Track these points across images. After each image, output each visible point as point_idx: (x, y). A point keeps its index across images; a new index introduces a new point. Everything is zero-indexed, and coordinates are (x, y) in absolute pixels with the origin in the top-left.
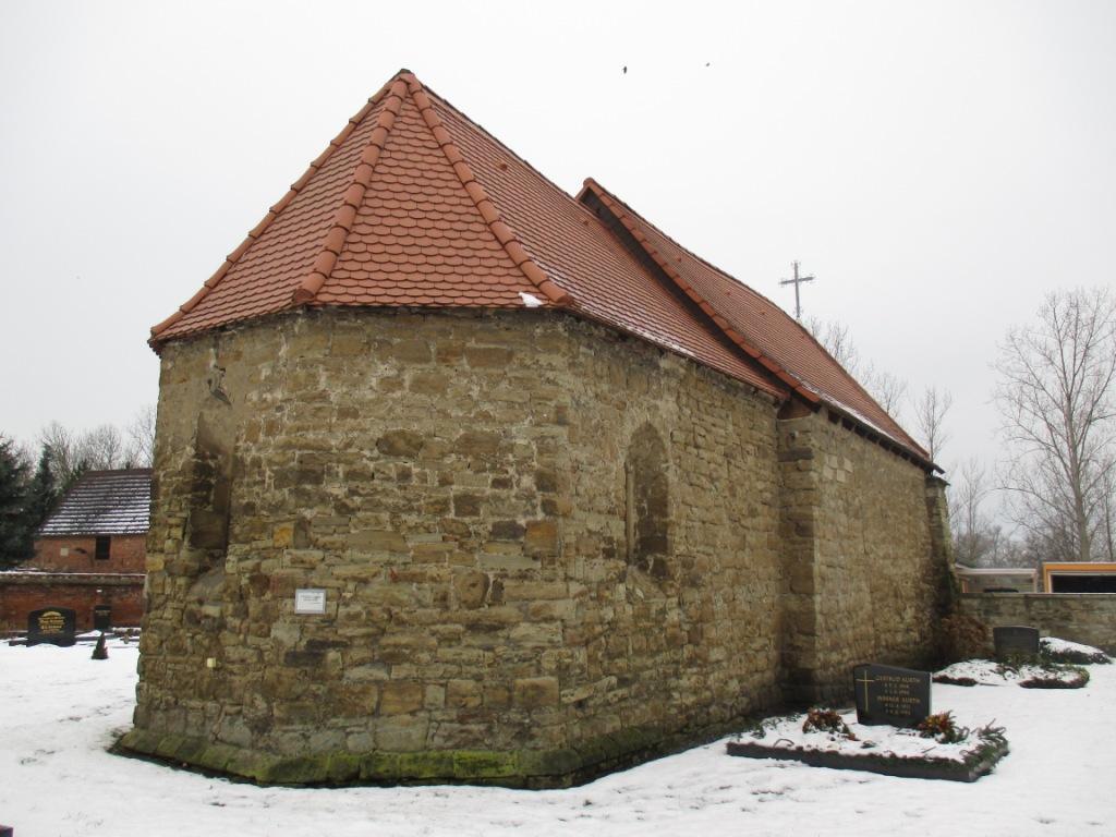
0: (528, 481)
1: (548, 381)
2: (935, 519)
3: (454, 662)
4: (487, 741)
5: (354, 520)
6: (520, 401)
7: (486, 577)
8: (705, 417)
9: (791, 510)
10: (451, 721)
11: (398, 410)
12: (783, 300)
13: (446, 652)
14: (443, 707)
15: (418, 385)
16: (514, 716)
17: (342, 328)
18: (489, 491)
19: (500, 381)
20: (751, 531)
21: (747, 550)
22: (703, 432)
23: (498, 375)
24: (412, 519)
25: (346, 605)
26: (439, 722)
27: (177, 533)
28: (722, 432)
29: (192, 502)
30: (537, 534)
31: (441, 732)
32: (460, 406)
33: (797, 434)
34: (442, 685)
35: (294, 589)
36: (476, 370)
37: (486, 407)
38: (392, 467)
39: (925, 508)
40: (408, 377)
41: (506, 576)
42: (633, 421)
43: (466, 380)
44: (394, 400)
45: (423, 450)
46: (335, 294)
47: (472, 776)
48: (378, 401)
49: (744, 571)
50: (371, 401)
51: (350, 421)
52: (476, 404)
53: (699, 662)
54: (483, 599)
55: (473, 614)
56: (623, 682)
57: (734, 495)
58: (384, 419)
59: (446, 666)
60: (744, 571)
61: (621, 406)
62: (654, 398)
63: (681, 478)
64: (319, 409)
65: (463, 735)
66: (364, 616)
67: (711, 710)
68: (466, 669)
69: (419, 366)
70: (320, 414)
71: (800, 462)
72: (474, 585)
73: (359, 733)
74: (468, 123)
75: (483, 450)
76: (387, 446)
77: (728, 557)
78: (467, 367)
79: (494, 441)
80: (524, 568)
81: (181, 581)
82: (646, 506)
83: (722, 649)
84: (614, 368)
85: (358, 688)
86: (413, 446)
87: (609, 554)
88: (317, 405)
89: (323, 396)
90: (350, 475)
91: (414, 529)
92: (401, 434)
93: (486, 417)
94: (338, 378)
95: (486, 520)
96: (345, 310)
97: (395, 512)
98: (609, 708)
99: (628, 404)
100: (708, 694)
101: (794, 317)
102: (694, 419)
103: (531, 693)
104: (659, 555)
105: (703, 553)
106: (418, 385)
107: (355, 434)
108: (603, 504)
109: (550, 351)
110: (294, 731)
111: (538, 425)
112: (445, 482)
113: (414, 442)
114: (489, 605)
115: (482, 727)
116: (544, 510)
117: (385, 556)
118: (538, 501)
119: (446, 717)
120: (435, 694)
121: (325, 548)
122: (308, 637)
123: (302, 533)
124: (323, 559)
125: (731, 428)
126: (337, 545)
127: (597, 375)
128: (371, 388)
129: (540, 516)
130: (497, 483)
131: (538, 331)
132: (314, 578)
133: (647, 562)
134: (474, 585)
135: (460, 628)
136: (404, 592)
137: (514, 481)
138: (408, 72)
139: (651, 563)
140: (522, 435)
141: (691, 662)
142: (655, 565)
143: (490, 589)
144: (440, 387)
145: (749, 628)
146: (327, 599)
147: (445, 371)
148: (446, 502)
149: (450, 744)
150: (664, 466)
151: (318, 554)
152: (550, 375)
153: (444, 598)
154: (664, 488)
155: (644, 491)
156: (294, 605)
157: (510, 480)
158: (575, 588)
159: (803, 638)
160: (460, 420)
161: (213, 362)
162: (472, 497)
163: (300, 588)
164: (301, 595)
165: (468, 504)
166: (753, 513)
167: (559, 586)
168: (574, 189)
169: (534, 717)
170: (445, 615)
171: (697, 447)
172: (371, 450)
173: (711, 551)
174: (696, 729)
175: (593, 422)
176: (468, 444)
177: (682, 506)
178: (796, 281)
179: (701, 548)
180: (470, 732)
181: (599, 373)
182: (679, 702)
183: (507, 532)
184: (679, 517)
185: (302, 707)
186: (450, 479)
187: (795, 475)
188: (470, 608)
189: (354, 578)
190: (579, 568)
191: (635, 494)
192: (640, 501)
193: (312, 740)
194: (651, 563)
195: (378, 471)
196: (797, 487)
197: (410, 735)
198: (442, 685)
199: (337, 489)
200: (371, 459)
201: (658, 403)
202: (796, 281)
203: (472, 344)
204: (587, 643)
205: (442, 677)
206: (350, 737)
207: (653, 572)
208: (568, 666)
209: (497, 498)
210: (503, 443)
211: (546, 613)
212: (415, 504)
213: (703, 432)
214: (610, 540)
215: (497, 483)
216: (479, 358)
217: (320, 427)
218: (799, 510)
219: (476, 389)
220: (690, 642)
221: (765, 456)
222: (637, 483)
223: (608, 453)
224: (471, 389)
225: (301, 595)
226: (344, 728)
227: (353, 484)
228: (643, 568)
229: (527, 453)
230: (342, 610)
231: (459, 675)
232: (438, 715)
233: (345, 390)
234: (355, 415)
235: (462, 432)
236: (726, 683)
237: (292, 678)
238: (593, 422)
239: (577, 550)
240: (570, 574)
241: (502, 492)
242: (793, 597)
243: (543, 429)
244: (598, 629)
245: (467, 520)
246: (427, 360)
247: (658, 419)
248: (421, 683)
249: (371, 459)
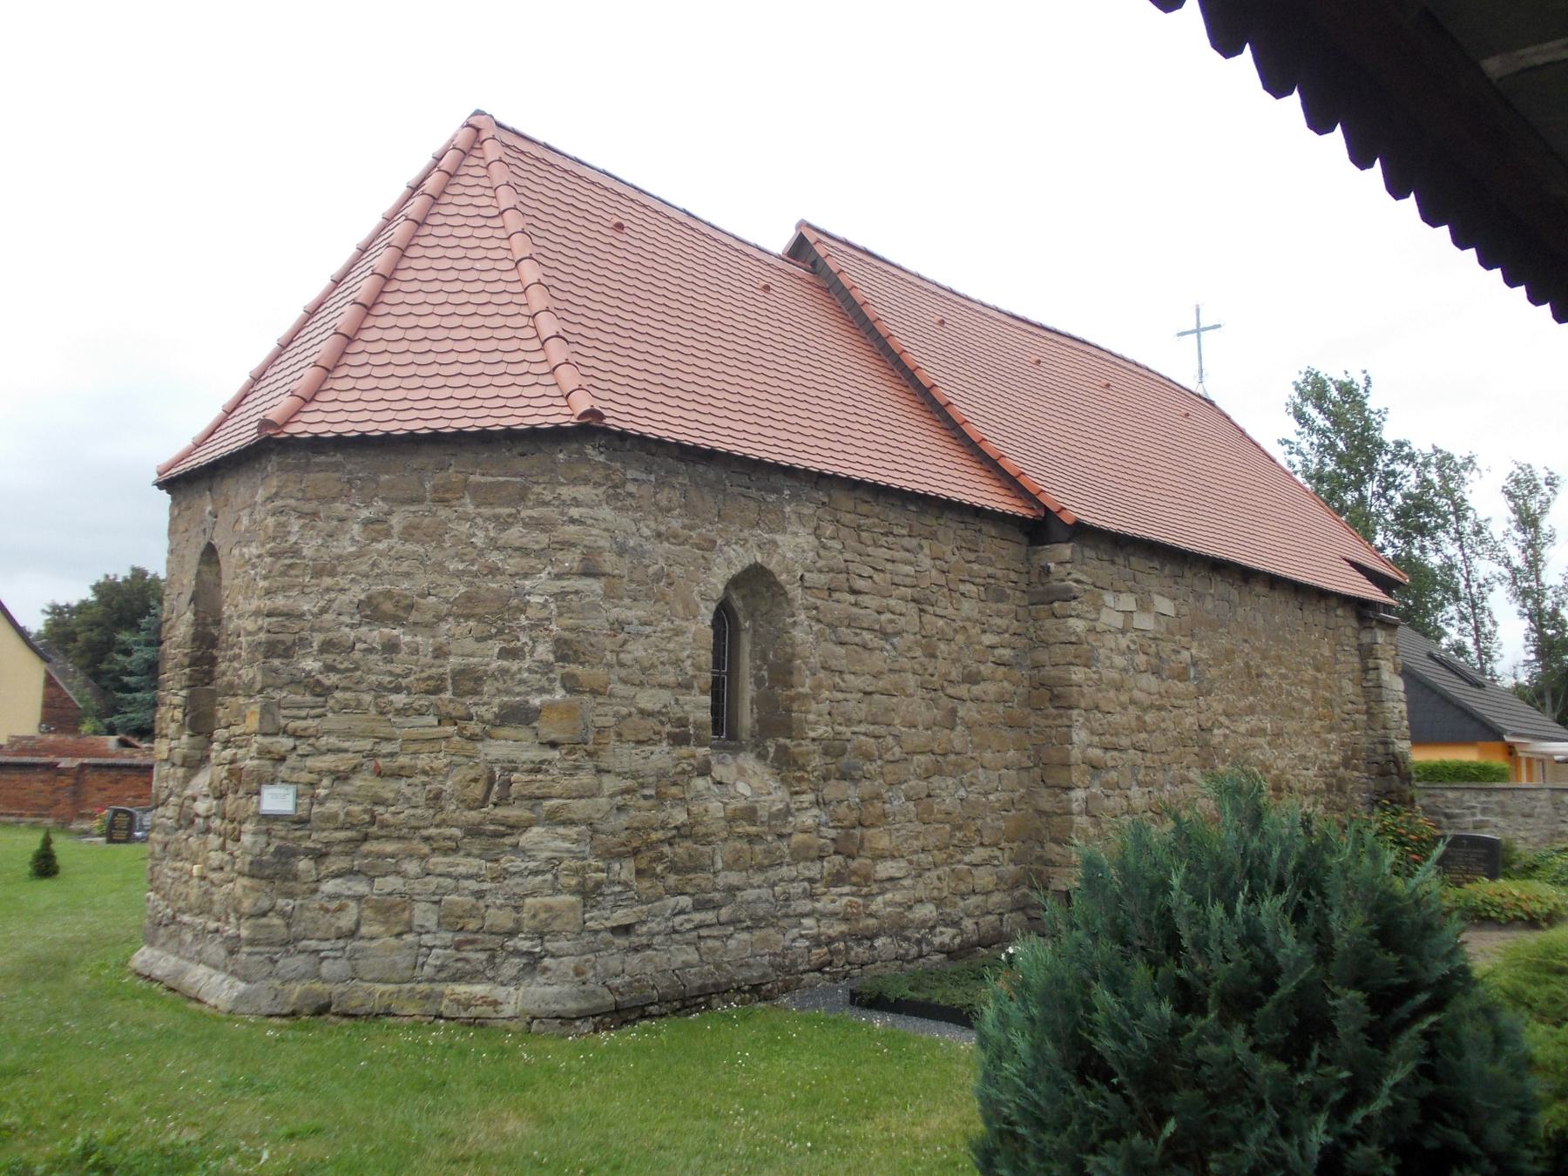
0: (544, 651)
1: (572, 521)
2: (1372, 675)
3: (449, 875)
4: (489, 974)
5: (331, 702)
6: (536, 547)
7: (492, 772)
8: (870, 550)
9: (1044, 672)
10: (446, 947)
11: (385, 563)
12: (1177, 366)
13: (438, 862)
14: (434, 928)
15: (408, 534)
16: (525, 945)
17: (317, 464)
18: (495, 664)
19: (512, 524)
20: (969, 704)
21: (959, 728)
22: (867, 571)
23: (510, 515)
24: (400, 699)
25: (321, 804)
26: (431, 948)
27: (178, 714)
28: (909, 569)
29: (190, 678)
30: (555, 716)
31: (430, 961)
32: (461, 557)
33: (1052, 565)
34: (435, 902)
35: (260, 784)
36: (482, 510)
37: (494, 557)
38: (377, 635)
39: (1357, 659)
40: (396, 522)
41: (515, 770)
42: (729, 562)
43: (470, 524)
44: (377, 551)
45: (414, 612)
46: (308, 425)
47: (464, 1014)
48: (359, 555)
49: (952, 757)
50: (351, 554)
51: (327, 581)
52: (481, 553)
53: (854, 879)
54: (486, 797)
55: (474, 816)
56: (700, 906)
57: (933, 656)
58: (366, 576)
59: (441, 879)
60: (952, 757)
61: (706, 545)
62: (771, 531)
63: (820, 636)
64: (291, 566)
65: (460, 965)
66: (342, 817)
67: (878, 943)
68: (466, 883)
69: (413, 508)
70: (293, 572)
71: (1056, 605)
72: (475, 780)
73: (335, 958)
74: (581, 171)
75: (496, 615)
76: (371, 611)
77: (919, 737)
78: (471, 509)
79: (503, 600)
80: (537, 759)
81: (180, 772)
82: (765, 674)
83: (903, 863)
84: (693, 494)
85: (334, 905)
86: (399, 611)
87: (679, 740)
88: (288, 562)
89: (295, 552)
90: (327, 646)
91: (402, 712)
92: (388, 595)
93: (494, 571)
94: (313, 528)
95: (487, 706)
96: (317, 444)
97: (379, 690)
98: (676, 937)
99: (719, 542)
100: (872, 922)
101: (1192, 385)
102: (848, 556)
103: (543, 916)
104: (782, 740)
105: (865, 734)
106: (408, 534)
107: (333, 595)
108: (671, 677)
109: (573, 482)
110: (261, 954)
111: (559, 577)
112: (440, 653)
113: (405, 602)
114: (495, 805)
115: (483, 956)
116: (564, 686)
117: (367, 744)
118: (558, 673)
119: (438, 943)
120: (423, 914)
121: (295, 735)
122: (276, 843)
123: (268, 717)
124: (295, 748)
125: (926, 563)
126: (310, 731)
127: (660, 510)
128: (352, 538)
129: (559, 695)
130: (505, 653)
131: (561, 456)
132: (283, 771)
133: (765, 748)
134: (475, 780)
135: (457, 832)
136: (388, 789)
137: (527, 649)
138: (483, 113)
139: (772, 750)
140: (539, 588)
141: (838, 879)
142: (777, 751)
143: (496, 788)
144: (437, 535)
145: (959, 835)
146: (298, 796)
147: (443, 513)
148: (441, 678)
149: (443, 975)
150: (790, 620)
151: (288, 743)
152: (575, 512)
153: (438, 796)
154: (788, 649)
155: (764, 658)
156: (259, 803)
157: (522, 649)
158: (610, 783)
159: (1057, 849)
160: (459, 574)
161: (209, 508)
162: (473, 671)
163: (267, 782)
164: (267, 792)
165: (469, 680)
166: (972, 678)
167: (585, 778)
168: (778, 241)
169: (547, 945)
170: (438, 818)
171: (853, 592)
172: (352, 616)
173: (882, 730)
174: (847, 967)
175: (650, 571)
176: (467, 607)
177: (822, 674)
178: (1198, 331)
179: (861, 728)
180: (466, 960)
181: (664, 503)
182: (815, 931)
183: (518, 715)
184: (818, 687)
185: (268, 926)
186: (445, 649)
187: (1050, 623)
188: (471, 809)
189: (331, 772)
190: (624, 756)
191: (752, 659)
192: (759, 669)
193: (279, 965)
194: (772, 750)
195: (359, 640)
196: (1052, 640)
197: (394, 963)
198: (435, 902)
199: (310, 664)
200: (352, 626)
201: (778, 538)
202: (1198, 331)
203: (476, 478)
204: (636, 852)
205: (434, 894)
206: (325, 963)
207: (775, 759)
208: (598, 885)
209: (504, 672)
210: (514, 602)
211: (565, 815)
212: (404, 682)
213: (867, 571)
214: (682, 722)
215: (505, 653)
216: (483, 495)
217: (292, 587)
218: (1054, 672)
219: (481, 534)
220: (836, 853)
221: (1001, 597)
222: (754, 644)
223: (679, 608)
224: (474, 535)
225: (267, 792)
226: (317, 952)
227: (329, 658)
228: (762, 756)
229: (545, 614)
230: (316, 809)
231: (456, 890)
232: (427, 939)
233: (320, 541)
234: (332, 574)
235: (462, 589)
236: (910, 907)
237: (1016, 885)
238: (650, 571)
239: (619, 735)
240: (603, 765)
241: (514, 666)
242: (1044, 791)
243: (565, 583)
244: (660, 835)
245: (469, 700)
246: (419, 500)
247: (776, 558)
248: (409, 899)
249: (352, 626)
